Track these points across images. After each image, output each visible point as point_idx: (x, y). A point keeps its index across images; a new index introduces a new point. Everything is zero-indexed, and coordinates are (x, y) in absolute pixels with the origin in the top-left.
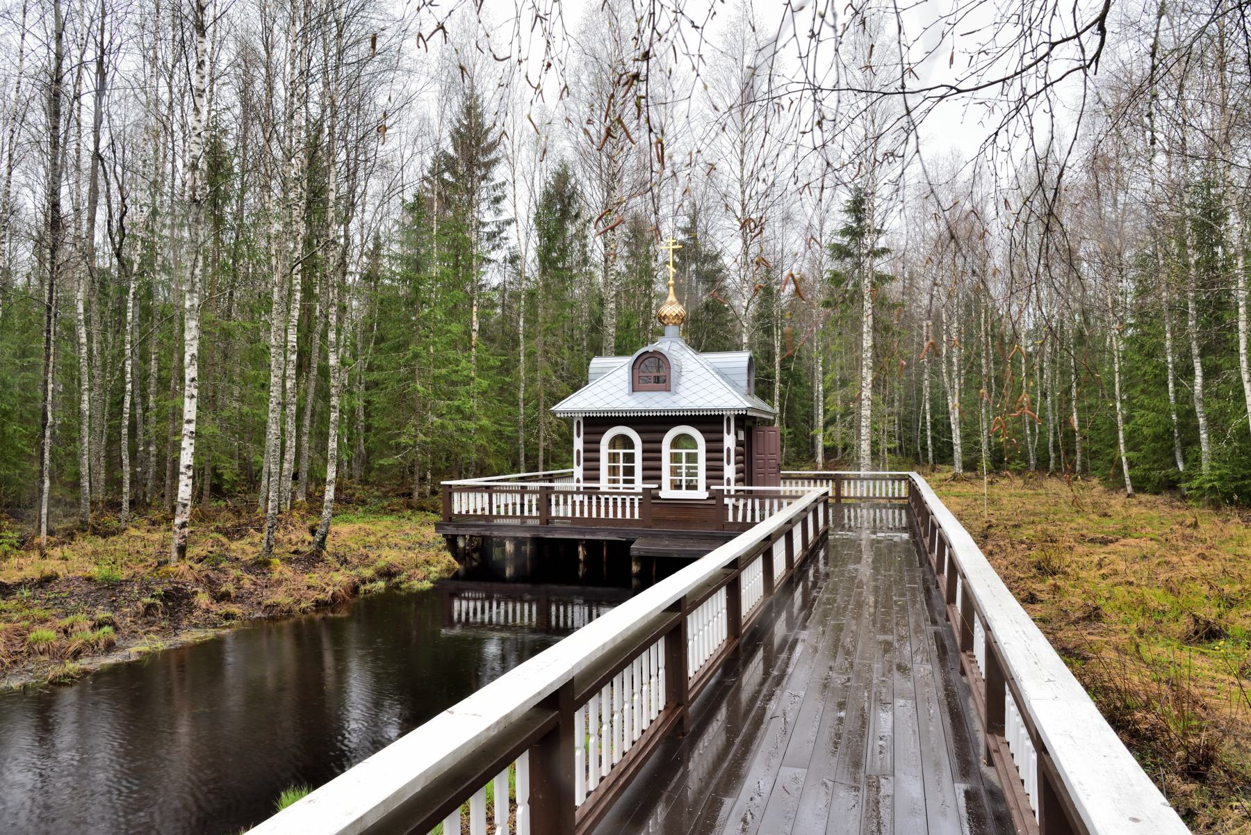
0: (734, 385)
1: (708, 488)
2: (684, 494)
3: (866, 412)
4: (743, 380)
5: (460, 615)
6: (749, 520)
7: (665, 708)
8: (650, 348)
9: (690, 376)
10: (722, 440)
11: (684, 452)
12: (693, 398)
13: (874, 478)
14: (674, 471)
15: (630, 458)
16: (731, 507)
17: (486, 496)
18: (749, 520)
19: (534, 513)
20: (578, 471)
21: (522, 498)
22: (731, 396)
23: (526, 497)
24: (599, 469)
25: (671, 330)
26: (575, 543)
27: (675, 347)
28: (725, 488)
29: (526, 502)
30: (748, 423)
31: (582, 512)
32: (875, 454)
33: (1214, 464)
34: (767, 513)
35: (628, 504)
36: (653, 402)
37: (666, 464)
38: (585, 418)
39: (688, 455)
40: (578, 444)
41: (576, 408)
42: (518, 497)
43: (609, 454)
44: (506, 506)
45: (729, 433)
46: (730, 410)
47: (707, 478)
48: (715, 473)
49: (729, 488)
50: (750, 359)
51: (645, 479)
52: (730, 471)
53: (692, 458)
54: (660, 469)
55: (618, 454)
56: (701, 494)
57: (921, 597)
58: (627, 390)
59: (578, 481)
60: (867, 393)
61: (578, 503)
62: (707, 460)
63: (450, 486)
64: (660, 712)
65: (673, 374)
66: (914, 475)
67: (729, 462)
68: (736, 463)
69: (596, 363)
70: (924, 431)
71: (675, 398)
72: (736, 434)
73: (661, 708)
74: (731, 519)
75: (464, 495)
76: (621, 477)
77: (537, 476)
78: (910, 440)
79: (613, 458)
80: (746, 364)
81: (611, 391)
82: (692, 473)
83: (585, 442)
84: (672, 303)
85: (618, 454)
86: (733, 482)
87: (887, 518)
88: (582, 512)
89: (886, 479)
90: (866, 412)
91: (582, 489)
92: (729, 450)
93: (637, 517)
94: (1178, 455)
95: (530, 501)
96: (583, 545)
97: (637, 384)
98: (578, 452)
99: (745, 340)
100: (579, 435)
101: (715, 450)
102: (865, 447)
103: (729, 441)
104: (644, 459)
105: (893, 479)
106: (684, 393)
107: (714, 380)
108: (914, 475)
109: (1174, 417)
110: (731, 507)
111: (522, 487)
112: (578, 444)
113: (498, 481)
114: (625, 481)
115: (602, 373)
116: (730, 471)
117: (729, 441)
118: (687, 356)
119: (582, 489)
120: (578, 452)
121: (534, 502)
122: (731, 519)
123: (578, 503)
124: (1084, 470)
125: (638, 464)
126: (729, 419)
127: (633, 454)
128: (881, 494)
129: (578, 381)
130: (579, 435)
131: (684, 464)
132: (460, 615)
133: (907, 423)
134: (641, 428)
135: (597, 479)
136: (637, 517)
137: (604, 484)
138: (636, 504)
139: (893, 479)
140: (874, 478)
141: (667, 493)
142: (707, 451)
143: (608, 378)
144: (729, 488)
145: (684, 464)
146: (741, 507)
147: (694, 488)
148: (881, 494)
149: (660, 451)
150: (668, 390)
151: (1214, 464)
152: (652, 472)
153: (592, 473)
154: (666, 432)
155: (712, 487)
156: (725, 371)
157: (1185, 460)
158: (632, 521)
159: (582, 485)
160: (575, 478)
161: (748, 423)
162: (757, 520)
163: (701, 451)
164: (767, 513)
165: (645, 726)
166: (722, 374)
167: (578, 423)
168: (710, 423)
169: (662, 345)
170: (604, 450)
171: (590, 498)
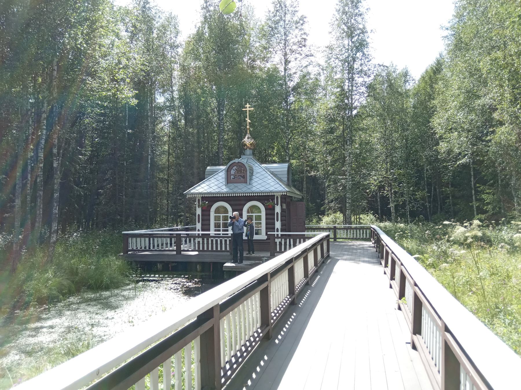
0: (281, 180)
1: (266, 234)
4: (286, 179)
8: (236, 160)
9: (258, 175)
12: (258, 187)
16: (278, 244)
17: (147, 239)
20: (199, 226)
22: (278, 185)
28: (276, 233)
30: (288, 200)
34: (288, 246)
35: (223, 243)
36: (241, 189)
40: (199, 211)
42: (169, 240)
46: (278, 192)
47: (266, 228)
48: (270, 226)
49: (277, 233)
52: (278, 225)
53: (259, 218)
57: (147, 283)
59: (278, 231)
67: (277, 220)
68: (281, 221)
71: (249, 187)
72: (281, 206)
75: (134, 239)
76: (221, 229)
77: (173, 229)
79: (217, 218)
81: (263, 184)
86: (280, 230)
89: (353, 229)
91: (280, 236)
97: (229, 181)
103: (278, 209)
104: (266, 219)
106: (254, 184)
107: (270, 177)
110: (278, 244)
111: (170, 234)
114: (223, 231)
116: (278, 225)
117: (278, 209)
118: (256, 165)
119: (280, 236)
126: (277, 197)
127: (260, 216)
129: (201, 178)
134: (232, 203)
136: (228, 249)
137: (212, 232)
138: (228, 243)
143: (215, 177)
144: (277, 233)
146: (283, 243)
150: (246, 182)
153: (206, 226)
155: (268, 233)
156: (276, 173)
160: (197, 230)
161: (288, 200)
162: (283, 250)
163: (263, 214)
164: (288, 246)
167: (199, 200)
169: (243, 160)
170: (212, 215)
171: (203, 240)
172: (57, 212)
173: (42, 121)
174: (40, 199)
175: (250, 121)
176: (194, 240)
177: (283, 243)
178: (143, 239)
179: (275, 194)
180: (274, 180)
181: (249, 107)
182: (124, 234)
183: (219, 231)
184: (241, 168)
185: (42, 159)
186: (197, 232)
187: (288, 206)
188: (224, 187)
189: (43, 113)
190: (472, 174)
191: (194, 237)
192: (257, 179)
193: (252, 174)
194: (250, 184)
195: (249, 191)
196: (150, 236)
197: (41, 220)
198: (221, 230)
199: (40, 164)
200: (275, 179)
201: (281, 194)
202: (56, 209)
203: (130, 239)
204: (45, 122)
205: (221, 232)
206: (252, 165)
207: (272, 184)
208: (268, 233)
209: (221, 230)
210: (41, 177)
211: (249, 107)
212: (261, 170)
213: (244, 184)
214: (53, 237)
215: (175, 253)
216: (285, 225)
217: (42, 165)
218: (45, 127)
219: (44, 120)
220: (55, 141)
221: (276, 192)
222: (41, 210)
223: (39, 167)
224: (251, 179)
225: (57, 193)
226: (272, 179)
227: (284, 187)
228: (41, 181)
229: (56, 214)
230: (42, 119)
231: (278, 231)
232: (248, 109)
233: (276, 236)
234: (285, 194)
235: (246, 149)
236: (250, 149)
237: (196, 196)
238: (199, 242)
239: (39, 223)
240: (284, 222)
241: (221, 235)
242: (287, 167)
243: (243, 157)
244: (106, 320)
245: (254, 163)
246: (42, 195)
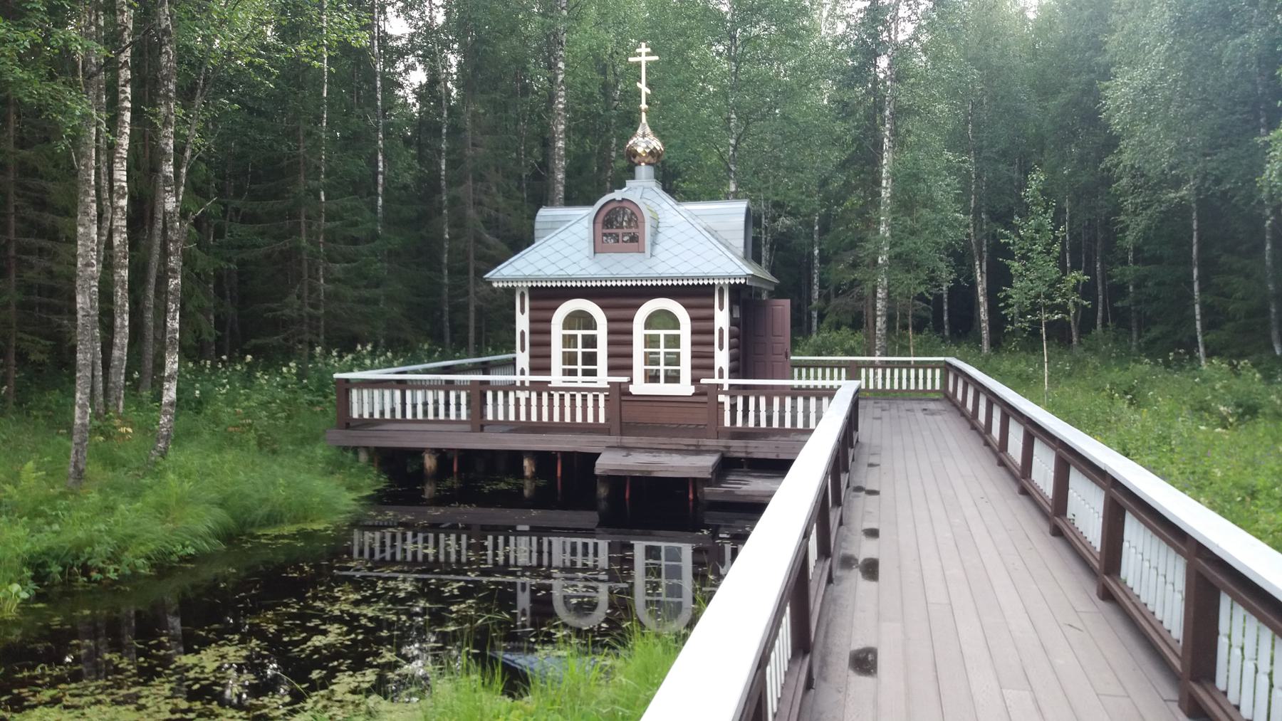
2: (580, 380)
4: (739, 241)
10: (712, 318)
11: (662, 333)
14: (650, 360)
16: (727, 407)
20: (523, 359)
24: (549, 356)
25: (644, 171)
27: (649, 194)
47: (694, 367)
48: (703, 362)
52: (722, 359)
53: (674, 341)
54: (630, 356)
56: (685, 388)
58: (587, 254)
63: (347, 381)
68: (730, 348)
82: (674, 360)
91: (527, 384)
92: (721, 331)
93: (602, 420)
98: (523, 333)
100: (721, 308)
101: (703, 331)
104: (693, 344)
107: (702, 239)
109: (1271, 287)
111: (448, 382)
112: (523, 322)
115: (554, 225)
117: (722, 319)
119: (527, 384)
120: (523, 333)
125: (602, 350)
129: (521, 240)
131: (662, 350)
134: (607, 302)
137: (556, 378)
142: (694, 332)
143: (562, 236)
145: (662, 350)
147: (673, 378)
149: (630, 333)
152: (620, 363)
153: (541, 364)
163: (685, 331)
172: (177, 326)
173: (120, 89)
174: (123, 288)
175: (649, 92)
176: (506, 395)
178: (387, 393)
179: (716, 282)
181: (647, 54)
182: (339, 380)
183: (573, 373)
185: (123, 187)
186: (518, 378)
187: (744, 312)
188: (585, 263)
189: (122, 68)
190: (1195, 227)
191: (512, 387)
193: (656, 231)
194: (652, 255)
195: (653, 273)
196: (402, 385)
197: (126, 341)
198: (580, 372)
199: (119, 199)
201: (732, 282)
202: (174, 318)
203: (354, 393)
204: (128, 90)
205: (580, 377)
206: (654, 205)
209: (580, 372)
210: (122, 232)
211: (647, 54)
213: (637, 255)
214: (168, 389)
215: (727, 423)
217: (124, 202)
218: (129, 105)
219: (124, 86)
220: (167, 144)
222: (126, 317)
223: (117, 207)
224: (654, 244)
225: (175, 278)
228: (122, 243)
229: (174, 331)
230: (121, 83)
231: (721, 376)
232: (643, 60)
234: (743, 281)
235: (639, 164)
236: (648, 164)
237: (515, 285)
238: (517, 400)
239: (123, 349)
242: (744, 211)
243: (629, 183)
245: (658, 200)
246: (126, 278)
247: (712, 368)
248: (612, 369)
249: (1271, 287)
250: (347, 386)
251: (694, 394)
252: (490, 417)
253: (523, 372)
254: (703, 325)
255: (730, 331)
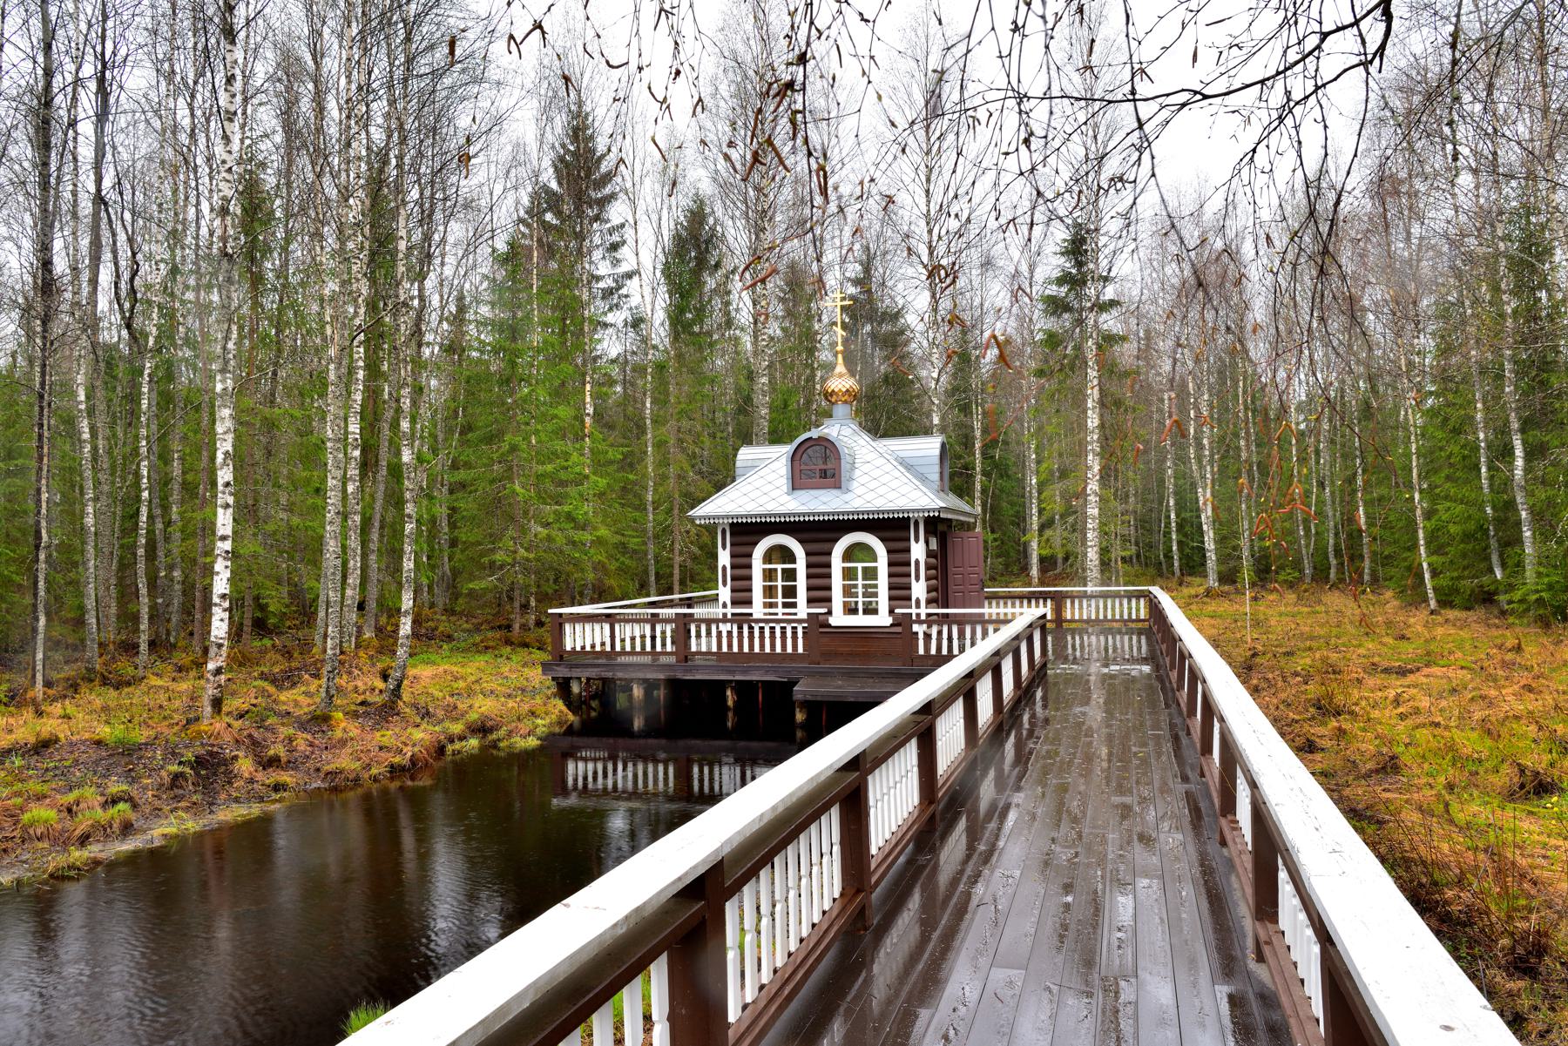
0: (923, 478)
1: (891, 612)
3: (1093, 511)
4: (934, 474)
5: (576, 780)
6: (945, 651)
7: (842, 895)
10: (908, 550)
11: (860, 566)
12: (869, 497)
13: (1105, 596)
14: (848, 591)
15: (790, 575)
16: (921, 636)
17: (607, 627)
18: (945, 651)
19: (669, 648)
20: (725, 593)
21: (653, 629)
23: (658, 628)
24: (751, 590)
25: (840, 410)
26: (721, 685)
27: (847, 431)
29: (658, 634)
30: (941, 528)
31: (730, 645)
32: (1105, 564)
33: (1541, 569)
34: (968, 642)
37: (758, 583)
38: (732, 525)
39: (864, 569)
40: (724, 558)
41: (720, 512)
42: (648, 628)
43: (764, 570)
44: (633, 639)
45: (917, 540)
47: (891, 598)
48: (900, 593)
49: (918, 611)
50: (943, 445)
51: (810, 601)
52: (919, 589)
53: (871, 574)
55: (776, 570)
56: (883, 619)
58: (785, 488)
60: (1093, 486)
61: (724, 634)
62: (890, 575)
63: (560, 615)
64: (834, 900)
65: (845, 466)
66: (1156, 590)
67: (917, 579)
68: (928, 579)
69: (745, 454)
70: (1167, 534)
71: (847, 497)
72: (927, 542)
73: (837, 895)
74: (921, 651)
76: (780, 600)
77: (672, 601)
78: (1150, 546)
79: (769, 575)
80: (937, 452)
82: (871, 593)
83: (732, 556)
84: (841, 376)
85: (776, 570)
86: (923, 603)
87: (1123, 647)
88: (730, 645)
90: (1093, 511)
91: (729, 616)
92: (917, 562)
93: (800, 650)
94: (1495, 558)
95: (663, 633)
96: (732, 689)
97: (799, 480)
98: (724, 568)
99: (936, 420)
100: (724, 547)
101: (899, 564)
102: (1093, 555)
103: (918, 551)
104: (809, 577)
105: (1129, 596)
107: (897, 474)
108: (1156, 590)
110: (921, 636)
111: (653, 615)
112: (724, 558)
113: (621, 607)
114: (785, 605)
115: (752, 466)
116: (919, 589)
117: (918, 551)
119: (729, 616)
120: (724, 568)
121: (669, 634)
122: (921, 651)
123: (724, 634)
124: (1375, 580)
126: (916, 523)
127: (794, 570)
128: (1114, 615)
129: (722, 476)
130: (724, 547)
131: (860, 582)
132: (576, 780)
133: (1147, 523)
134: (805, 536)
135: (749, 603)
136: (800, 650)
137: (757, 610)
138: (800, 634)
139: (1129, 596)
140: (1105, 596)
141: (839, 619)
142: (890, 565)
144: (918, 611)
145: (860, 582)
146: (934, 636)
147: (870, 610)
148: (1114, 615)
149: (829, 566)
150: (838, 486)
151: (1541, 569)
152: (820, 594)
153: (742, 596)
154: (756, 544)
155: (897, 611)
157: (1504, 565)
158: (795, 655)
159: (730, 611)
160: (721, 602)
161: (941, 528)
162: (956, 651)
163: (801, 566)
164: (968, 642)
165: (881, 844)
166: (907, 465)
167: (724, 532)
168: (892, 528)
170: (758, 566)
171: (740, 628)
177: (934, 636)
180: (906, 481)
184: (827, 447)
187: (943, 544)
192: (865, 479)
196: (610, 618)
198: (780, 605)
200: (910, 477)
203: (568, 628)
207: (904, 490)
208: (897, 611)
212: (874, 455)
213: (835, 492)
216: (936, 590)
221: (913, 511)
222: (358, 559)
226: (904, 479)
227: (933, 497)
233: (914, 617)
240: (934, 582)
241: (780, 617)
242: (938, 445)
244: (45, 735)
247: (910, 599)
248: (811, 601)
249: (1489, 510)
250: (560, 621)
251: (892, 625)
252: (694, 648)
253: (725, 606)
254: (899, 557)
255: (926, 563)
